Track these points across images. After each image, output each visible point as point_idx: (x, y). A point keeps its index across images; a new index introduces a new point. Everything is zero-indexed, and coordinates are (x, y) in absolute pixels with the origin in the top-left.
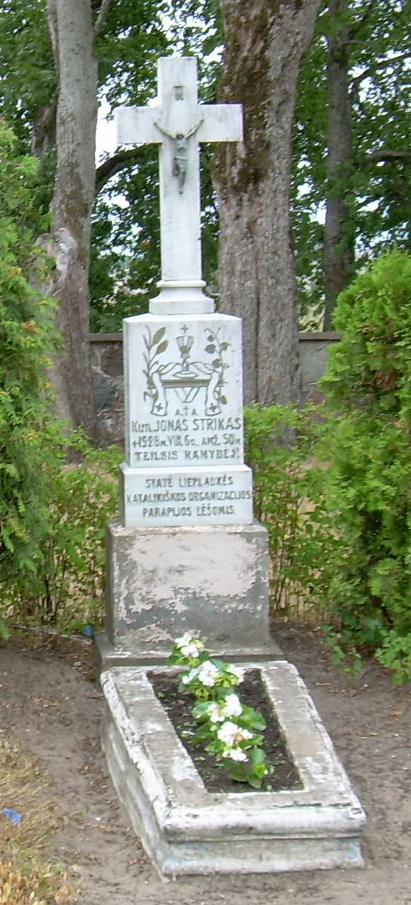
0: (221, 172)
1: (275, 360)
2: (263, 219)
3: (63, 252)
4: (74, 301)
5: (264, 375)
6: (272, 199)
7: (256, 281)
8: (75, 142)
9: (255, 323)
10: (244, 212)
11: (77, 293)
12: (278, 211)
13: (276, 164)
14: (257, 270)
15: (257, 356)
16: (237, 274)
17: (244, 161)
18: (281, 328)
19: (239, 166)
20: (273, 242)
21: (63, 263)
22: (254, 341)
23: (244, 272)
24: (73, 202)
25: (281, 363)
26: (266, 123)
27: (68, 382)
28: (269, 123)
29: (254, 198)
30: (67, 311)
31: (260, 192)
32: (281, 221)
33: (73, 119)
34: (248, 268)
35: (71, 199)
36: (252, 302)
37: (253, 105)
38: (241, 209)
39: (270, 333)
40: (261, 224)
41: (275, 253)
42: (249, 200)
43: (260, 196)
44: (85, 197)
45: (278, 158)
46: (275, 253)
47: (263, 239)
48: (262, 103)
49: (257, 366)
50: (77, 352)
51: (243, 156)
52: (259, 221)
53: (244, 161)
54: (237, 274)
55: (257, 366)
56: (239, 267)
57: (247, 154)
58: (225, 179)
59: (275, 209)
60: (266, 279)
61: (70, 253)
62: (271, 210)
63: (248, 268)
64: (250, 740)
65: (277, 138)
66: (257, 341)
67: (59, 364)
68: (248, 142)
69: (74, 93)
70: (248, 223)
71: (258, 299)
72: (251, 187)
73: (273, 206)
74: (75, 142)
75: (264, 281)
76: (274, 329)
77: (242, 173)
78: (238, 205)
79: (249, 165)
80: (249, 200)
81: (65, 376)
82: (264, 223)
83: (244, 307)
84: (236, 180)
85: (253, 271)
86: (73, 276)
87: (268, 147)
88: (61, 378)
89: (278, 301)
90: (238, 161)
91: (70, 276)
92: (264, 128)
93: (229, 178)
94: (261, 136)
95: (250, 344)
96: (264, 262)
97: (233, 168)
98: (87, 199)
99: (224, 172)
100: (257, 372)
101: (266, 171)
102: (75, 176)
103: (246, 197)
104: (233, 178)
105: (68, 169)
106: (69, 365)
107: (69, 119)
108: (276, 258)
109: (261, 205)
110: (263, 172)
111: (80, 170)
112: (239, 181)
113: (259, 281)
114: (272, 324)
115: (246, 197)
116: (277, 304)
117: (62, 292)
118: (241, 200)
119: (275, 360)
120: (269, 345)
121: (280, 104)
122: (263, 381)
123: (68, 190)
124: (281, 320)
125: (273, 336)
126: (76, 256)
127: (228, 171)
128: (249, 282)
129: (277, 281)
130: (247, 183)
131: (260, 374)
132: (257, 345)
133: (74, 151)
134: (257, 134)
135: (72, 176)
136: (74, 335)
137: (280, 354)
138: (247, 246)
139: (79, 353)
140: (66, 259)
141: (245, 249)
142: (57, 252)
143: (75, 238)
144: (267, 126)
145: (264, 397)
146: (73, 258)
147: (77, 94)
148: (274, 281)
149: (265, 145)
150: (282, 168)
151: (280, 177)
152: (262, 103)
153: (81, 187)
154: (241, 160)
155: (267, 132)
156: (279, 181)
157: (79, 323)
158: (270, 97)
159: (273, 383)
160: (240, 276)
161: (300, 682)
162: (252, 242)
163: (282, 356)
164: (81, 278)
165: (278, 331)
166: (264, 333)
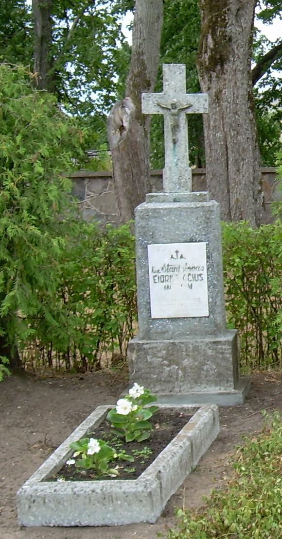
0: (199, 58)
1: (240, 187)
2: (226, 90)
3: (127, 114)
4: (133, 148)
5: (234, 198)
6: (233, 76)
7: (223, 133)
8: (142, 38)
9: (225, 161)
10: (213, 85)
11: (136, 142)
12: (238, 84)
13: (236, 51)
14: (223, 125)
15: (228, 184)
16: (211, 128)
17: (212, 50)
18: (243, 165)
19: (209, 53)
20: (234, 106)
21: (126, 121)
22: (226, 174)
23: (215, 126)
24: (138, 80)
25: (245, 189)
26: (227, 23)
27: (131, 203)
28: (230, 23)
29: (220, 76)
30: (129, 154)
31: (225, 71)
32: (240, 91)
33: (141, 23)
34: (217, 124)
35: (137, 77)
36: (221, 148)
37: (218, 11)
38: (211, 83)
39: (235, 169)
40: (225, 93)
41: (236, 113)
42: (216, 77)
43: (224, 74)
44: (148, 76)
45: (237, 48)
46: (236, 113)
47: (227, 103)
48: (224, 10)
49: (229, 192)
50: (137, 183)
51: (212, 46)
52: (223, 92)
53: (212, 50)
54: (211, 128)
55: (229, 192)
56: (212, 123)
57: (214, 46)
58: (201, 62)
59: (236, 83)
60: (230, 131)
61: (131, 114)
62: (232, 84)
63: (217, 124)
64: (68, 460)
65: (236, 34)
66: (228, 174)
67: (125, 191)
68: (215, 36)
69: (142, 4)
70: (216, 93)
71: (226, 145)
72: (219, 67)
73: (233, 81)
74: (142, 38)
75: (228, 132)
76: (239, 166)
77: (211, 58)
78: (208, 80)
79: (216, 52)
80: (216, 77)
81: (130, 199)
82: (227, 93)
83: (217, 151)
84: (207, 63)
85: (221, 126)
86: (133, 130)
87: (230, 40)
88: (126, 200)
89: (239, 146)
90: (208, 50)
91: (130, 131)
92: (225, 27)
93: (203, 62)
94: (223, 32)
95: (223, 176)
96: (227, 120)
97: (206, 55)
98: (149, 78)
99: (201, 57)
100: (229, 195)
101: (228, 57)
102: (140, 61)
103: (214, 75)
104: (205, 62)
105: (136, 57)
106: (132, 192)
107: (139, 22)
108: (237, 117)
109: (225, 80)
110: (226, 57)
111: (145, 57)
112: (209, 63)
113: (225, 132)
114: (236, 161)
115: (214, 75)
116: (239, 148)
117: (125, 141)
118: (211, 77)
119: (240, 187)
120: (236, 177)
121: (238, 10)
122: (233, 203)
123: (136, 71)
124: (243, 160)
125: (238, 171)
126: (134, 117)
127: (203, 56)
128: (219, 134)
129: (238, 133)
130: (216, 65)
131: (231, 197)
132: (228, 177)
133: (141, 44)
134: (220, 31)
135: (138, 61)
136: (135, 171)
137: (244, 183)
138: (216, 108)
139: (139, 182)
140: (128, 119)
141: (214, 111)
142: (124, 113)
143: (135, 104)
144: (228, 25)
145: (234, 213)
146: (132, 118)
147: (144, 5)
148: (236, 133)
149: (227, 38)
150: (240, 54)
151: (238, 60)
152: (224, 10)
153: (145, 69)
154: (210, 49)
155: (228, 30)
156: (237, 63)
157: (139, 163)
158: (229, 5)
159: (239, 203)
160: (213, 129)
161: (94, 422)
162: (219, 106)
163: (245, 184)
164: (138, 131)
165: (241, 167)
166: (232, 168)
